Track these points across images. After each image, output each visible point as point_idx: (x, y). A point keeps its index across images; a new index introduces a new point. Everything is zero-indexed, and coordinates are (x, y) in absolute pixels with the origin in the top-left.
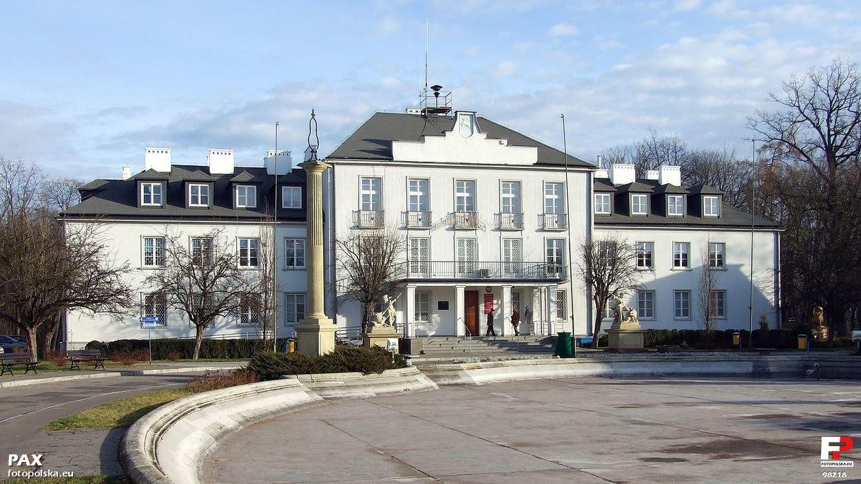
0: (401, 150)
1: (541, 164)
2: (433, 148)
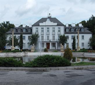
0: (41, 24)
1: (58, 25)
2: (44, 24)
